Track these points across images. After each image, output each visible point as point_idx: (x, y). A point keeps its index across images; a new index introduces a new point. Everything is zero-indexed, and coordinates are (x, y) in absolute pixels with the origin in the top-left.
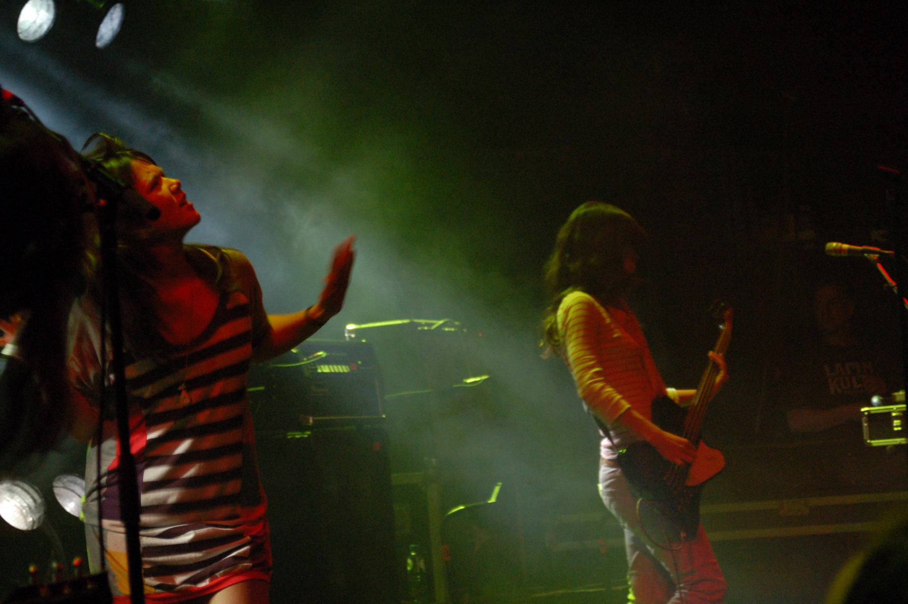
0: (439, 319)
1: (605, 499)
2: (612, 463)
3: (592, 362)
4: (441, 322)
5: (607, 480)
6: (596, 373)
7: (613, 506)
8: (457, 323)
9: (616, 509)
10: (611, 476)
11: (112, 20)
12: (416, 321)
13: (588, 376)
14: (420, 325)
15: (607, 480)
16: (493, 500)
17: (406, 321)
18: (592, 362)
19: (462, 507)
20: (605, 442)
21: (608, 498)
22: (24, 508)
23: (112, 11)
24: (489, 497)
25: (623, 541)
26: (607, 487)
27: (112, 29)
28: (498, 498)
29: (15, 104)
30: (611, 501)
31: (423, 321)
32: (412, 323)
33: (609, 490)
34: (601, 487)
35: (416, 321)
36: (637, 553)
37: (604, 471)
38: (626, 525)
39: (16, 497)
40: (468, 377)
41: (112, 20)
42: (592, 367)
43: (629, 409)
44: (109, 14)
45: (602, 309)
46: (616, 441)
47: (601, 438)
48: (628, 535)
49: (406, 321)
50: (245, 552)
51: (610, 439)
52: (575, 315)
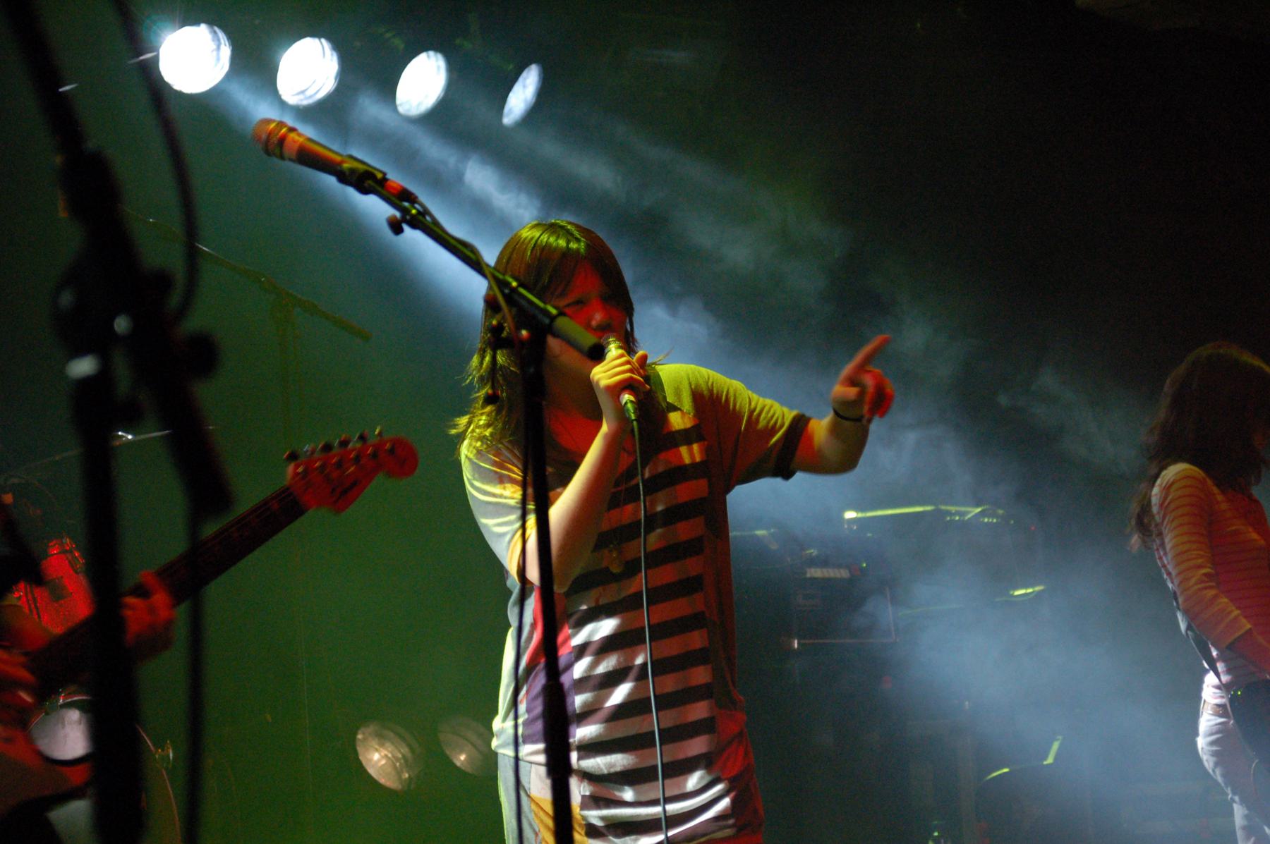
0: (978, 505)
1: (1208, 761)
2: (1221, 710)
3: (1200, 561)
4: (979, 510)
5: (1212, 734)
6: (1205, 575)
7: (1218, 771)
8: (1001, 512)
9: (1224, 776)
10: (1222, 730)
11: (524, 87)
12: (943, 507)
13: (1193, 581)
14: (949, 513)
15: (1212, 734)
16: (1050, 760)
17: (929, 508)
18: (1200, 561)
19: (1006, 770)
20: (1210, 679)
21: (1213, 759)
22: (397, 759)
23: (524, 74)
24: (1045, 758)
25: (1233, 822)
26: (1212, 743)
27: (526, 100)
28: (1056, 759)
29: (407, 201)
30: (1216, 764)
31: (953, 509)
32: (938, 511)
33: (1215, 748)
34: (1201, 742)
35: (943, 507)
36: (1253, 839)
37: (1207, 721)
38: (1237, 798)
39: (388, 744)
40: (1016, 588)
41: (524, 87)
42: (1200, 567)
43: (1249, 632)
44: (521, 79)
45: (1215, 490)
46: (1225, 678)
47: (1206, 671)
48: (1239, 812)
49: (929, 508)
50: (725, 810)
51: (1217, 674)
52: (1179, 493)
